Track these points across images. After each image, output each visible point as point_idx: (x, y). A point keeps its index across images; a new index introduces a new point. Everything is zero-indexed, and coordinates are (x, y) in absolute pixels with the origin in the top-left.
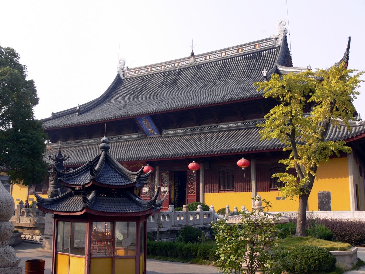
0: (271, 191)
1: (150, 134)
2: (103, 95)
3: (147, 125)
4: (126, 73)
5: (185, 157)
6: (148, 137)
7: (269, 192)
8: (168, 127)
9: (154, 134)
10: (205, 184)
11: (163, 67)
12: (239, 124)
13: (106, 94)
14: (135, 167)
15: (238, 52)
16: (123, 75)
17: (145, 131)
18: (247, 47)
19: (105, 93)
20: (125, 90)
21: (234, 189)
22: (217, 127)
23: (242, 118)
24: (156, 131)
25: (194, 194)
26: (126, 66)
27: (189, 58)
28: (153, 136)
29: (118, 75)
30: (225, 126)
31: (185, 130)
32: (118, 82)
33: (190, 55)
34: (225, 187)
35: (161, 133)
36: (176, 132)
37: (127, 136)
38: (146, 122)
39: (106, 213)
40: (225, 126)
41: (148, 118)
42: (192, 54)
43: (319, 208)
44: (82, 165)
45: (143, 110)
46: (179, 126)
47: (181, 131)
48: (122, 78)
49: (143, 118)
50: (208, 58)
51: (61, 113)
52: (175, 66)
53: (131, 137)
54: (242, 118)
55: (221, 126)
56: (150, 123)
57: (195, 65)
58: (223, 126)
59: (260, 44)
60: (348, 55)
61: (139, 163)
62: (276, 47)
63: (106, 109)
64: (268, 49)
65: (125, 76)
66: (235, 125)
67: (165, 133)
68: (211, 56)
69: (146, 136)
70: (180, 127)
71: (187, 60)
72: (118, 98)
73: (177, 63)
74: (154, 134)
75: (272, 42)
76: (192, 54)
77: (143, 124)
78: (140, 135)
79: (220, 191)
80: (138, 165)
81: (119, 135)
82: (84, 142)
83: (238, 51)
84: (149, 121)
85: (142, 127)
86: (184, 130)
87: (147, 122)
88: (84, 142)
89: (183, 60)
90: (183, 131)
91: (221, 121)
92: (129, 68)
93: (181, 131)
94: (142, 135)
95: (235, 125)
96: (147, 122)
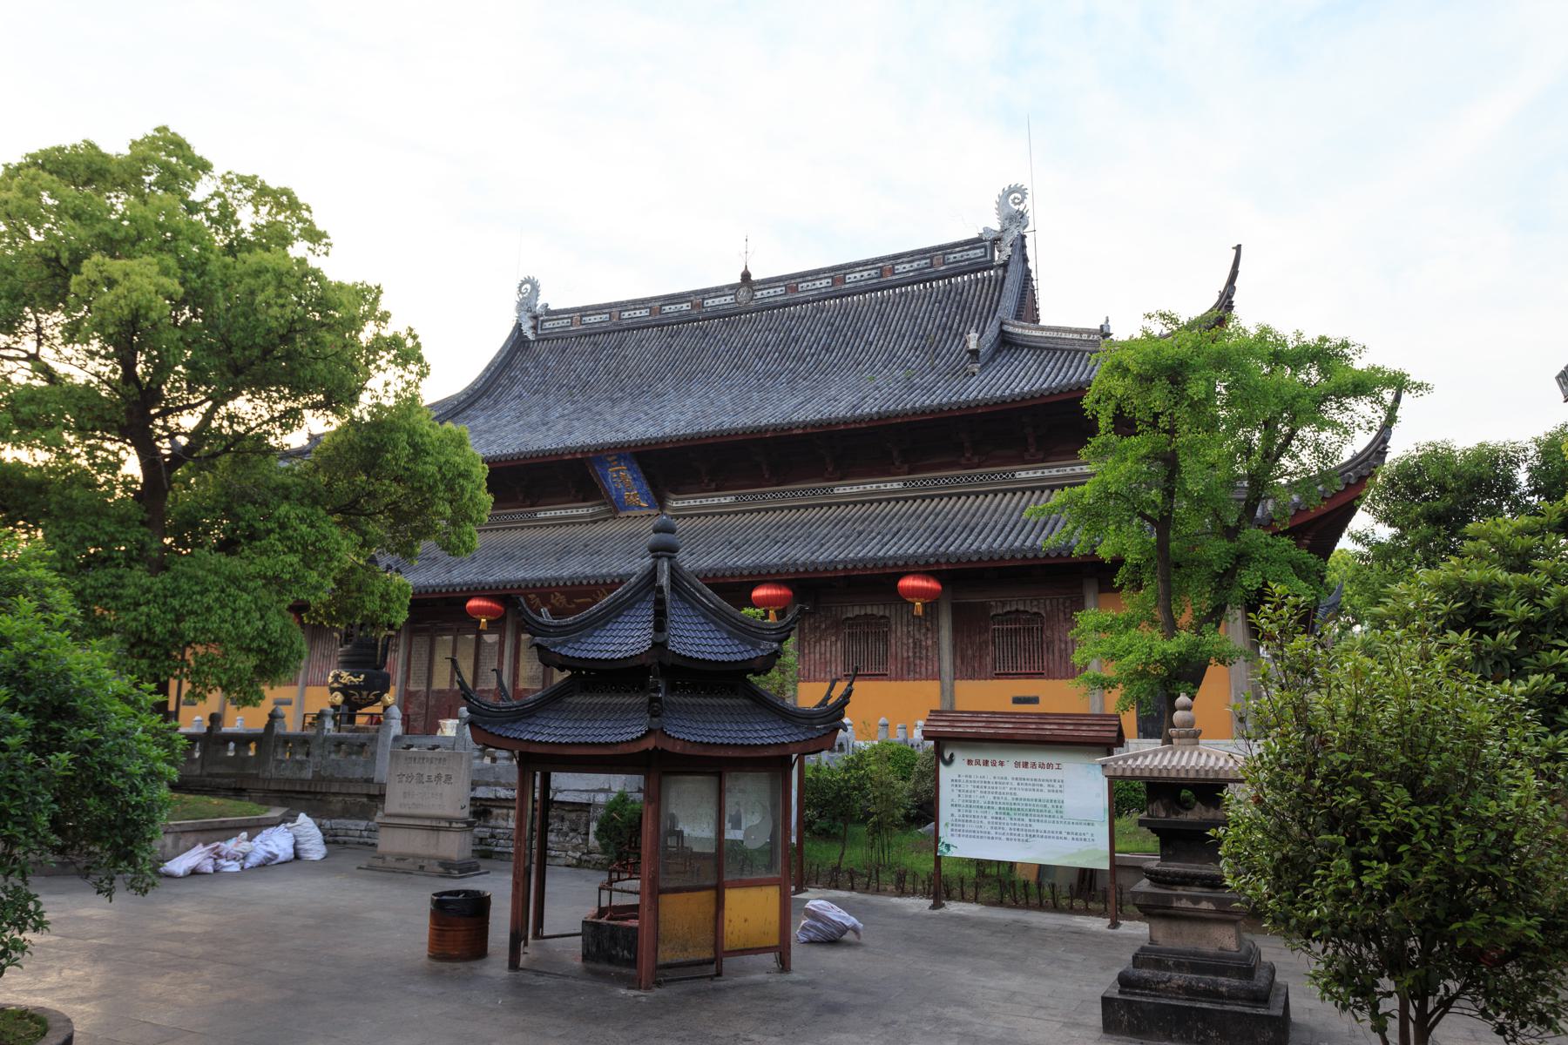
2: (474, 383)
3: (621, 479)
6: (623, 514)
12: (895, 486)
19: (480, 378)
23: (713, 486)
26: (540, 303)
27: (733, 288)
28: (636, 512)
29: (518, 327)
30: (855, 489)
32: (518, 343)
33: (738, 280)
35: (660, 502)
39: (607, 744)
40: (855, 489)
42: (746, 276)
43: (1139, 730)
44: (621, 583)
45: (610, 437)
46: (720, 484)
47: (723, 500)
53: (569, 512)
54: (713, 486)
58: (848, 490)
60: (1229, 296)
63: (484, 428)
64: (943, 278)
70: (720, 488)
72: (520, 396)
74: (641, 507)
76: (746, 276)
89: (718, 291)
90: (728, 500)
91: (1023, 460)
92: (552, 307)
93: (723, 500)
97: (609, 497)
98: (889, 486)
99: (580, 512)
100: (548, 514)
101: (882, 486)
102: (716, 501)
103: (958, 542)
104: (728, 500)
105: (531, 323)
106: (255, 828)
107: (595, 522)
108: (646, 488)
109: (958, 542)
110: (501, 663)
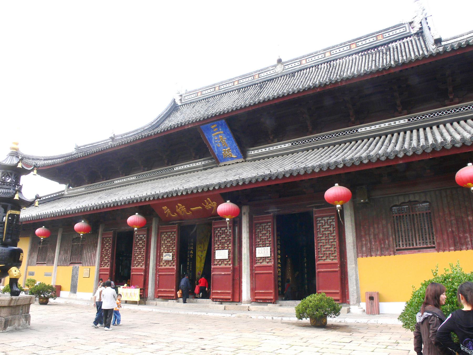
0: (399, 254)
1: (225, 160)
3: (220, 140)
4: (184, 97)
5: (319, 172)
6: (221, 164)
7: (442, 252)
8: (256, 143)
9: (232, 158)
10: (359, 237)
11: (236, 83)
12: (402, 122)
13: (155, 122)
14: (200, 209)
15: (197, 96)
16: (181, 100)
17: (216, 153)
18: (364, 40)
20: (182, 116)
21: (434, 244)
22: (357, 131)
24: (237, 152)
25: (141, 266)
27: (275, 66)
28: (230, 162)
29: (174, 101)
31: (292, 144)
33: (275, 63)
34: (423, 240)
36: (274, 149)
37: (182, 167)
38: (218, 135)
40: (373, 128)
41: (222, 125)
42: (280, 61)
47: (283, 146)
48: (179, 104)
49: (212, 127)
50: (304, 62)
51: (88, 146)
52: (254, 79)
55: (363, 129)
56: (226, 137)
57: (284, 74)
59: (384, 35)
61: (207, 201)
62: (412, 35)
65: (183, 101)
66: (395, 123)
67: (252, 152)
68: (307, 60)
69: (218, 163)
71: (272, 68)
73: (257, 75)
75: (404, 28)
76: (280, 61)
77: (213, 139)
78: (207, 162)
79: (397, 250)
80: (206, 204)
81: (172, 165)
82: (116, 182)
83: (350, 47)
84: (224, 133)
85: (212, 146)
86: (290, 144)
87: (220, 134)
88: (116, 182)
90: (287, 145)
94: (210, 161)
95: (395, 123)
96: (220, 134)
97: (214, 154)
98: (397, 123)
99: (197, 164)
100: (180, 168)
101: (392, 123)
102: (279, 147)
103: (356, 67)
104: (287, 145)
105: (180, 98)
106: (191, 127)
107: (206, 169)
108: (235, 144)
109: (356, 67)
110: (147, 265)
